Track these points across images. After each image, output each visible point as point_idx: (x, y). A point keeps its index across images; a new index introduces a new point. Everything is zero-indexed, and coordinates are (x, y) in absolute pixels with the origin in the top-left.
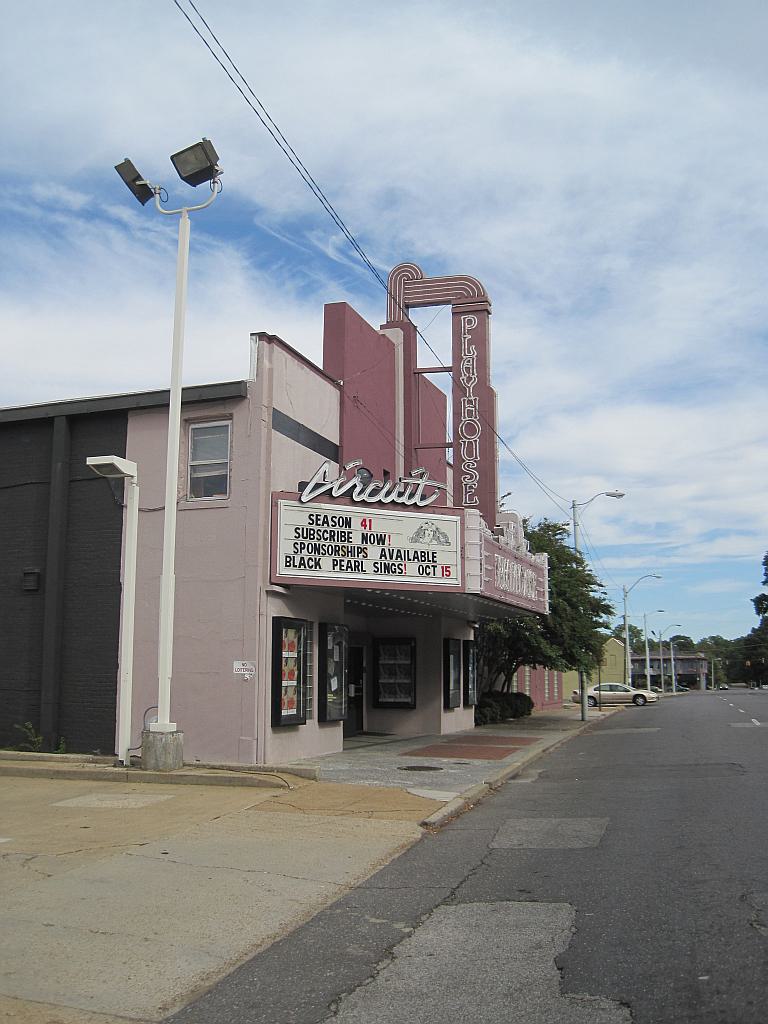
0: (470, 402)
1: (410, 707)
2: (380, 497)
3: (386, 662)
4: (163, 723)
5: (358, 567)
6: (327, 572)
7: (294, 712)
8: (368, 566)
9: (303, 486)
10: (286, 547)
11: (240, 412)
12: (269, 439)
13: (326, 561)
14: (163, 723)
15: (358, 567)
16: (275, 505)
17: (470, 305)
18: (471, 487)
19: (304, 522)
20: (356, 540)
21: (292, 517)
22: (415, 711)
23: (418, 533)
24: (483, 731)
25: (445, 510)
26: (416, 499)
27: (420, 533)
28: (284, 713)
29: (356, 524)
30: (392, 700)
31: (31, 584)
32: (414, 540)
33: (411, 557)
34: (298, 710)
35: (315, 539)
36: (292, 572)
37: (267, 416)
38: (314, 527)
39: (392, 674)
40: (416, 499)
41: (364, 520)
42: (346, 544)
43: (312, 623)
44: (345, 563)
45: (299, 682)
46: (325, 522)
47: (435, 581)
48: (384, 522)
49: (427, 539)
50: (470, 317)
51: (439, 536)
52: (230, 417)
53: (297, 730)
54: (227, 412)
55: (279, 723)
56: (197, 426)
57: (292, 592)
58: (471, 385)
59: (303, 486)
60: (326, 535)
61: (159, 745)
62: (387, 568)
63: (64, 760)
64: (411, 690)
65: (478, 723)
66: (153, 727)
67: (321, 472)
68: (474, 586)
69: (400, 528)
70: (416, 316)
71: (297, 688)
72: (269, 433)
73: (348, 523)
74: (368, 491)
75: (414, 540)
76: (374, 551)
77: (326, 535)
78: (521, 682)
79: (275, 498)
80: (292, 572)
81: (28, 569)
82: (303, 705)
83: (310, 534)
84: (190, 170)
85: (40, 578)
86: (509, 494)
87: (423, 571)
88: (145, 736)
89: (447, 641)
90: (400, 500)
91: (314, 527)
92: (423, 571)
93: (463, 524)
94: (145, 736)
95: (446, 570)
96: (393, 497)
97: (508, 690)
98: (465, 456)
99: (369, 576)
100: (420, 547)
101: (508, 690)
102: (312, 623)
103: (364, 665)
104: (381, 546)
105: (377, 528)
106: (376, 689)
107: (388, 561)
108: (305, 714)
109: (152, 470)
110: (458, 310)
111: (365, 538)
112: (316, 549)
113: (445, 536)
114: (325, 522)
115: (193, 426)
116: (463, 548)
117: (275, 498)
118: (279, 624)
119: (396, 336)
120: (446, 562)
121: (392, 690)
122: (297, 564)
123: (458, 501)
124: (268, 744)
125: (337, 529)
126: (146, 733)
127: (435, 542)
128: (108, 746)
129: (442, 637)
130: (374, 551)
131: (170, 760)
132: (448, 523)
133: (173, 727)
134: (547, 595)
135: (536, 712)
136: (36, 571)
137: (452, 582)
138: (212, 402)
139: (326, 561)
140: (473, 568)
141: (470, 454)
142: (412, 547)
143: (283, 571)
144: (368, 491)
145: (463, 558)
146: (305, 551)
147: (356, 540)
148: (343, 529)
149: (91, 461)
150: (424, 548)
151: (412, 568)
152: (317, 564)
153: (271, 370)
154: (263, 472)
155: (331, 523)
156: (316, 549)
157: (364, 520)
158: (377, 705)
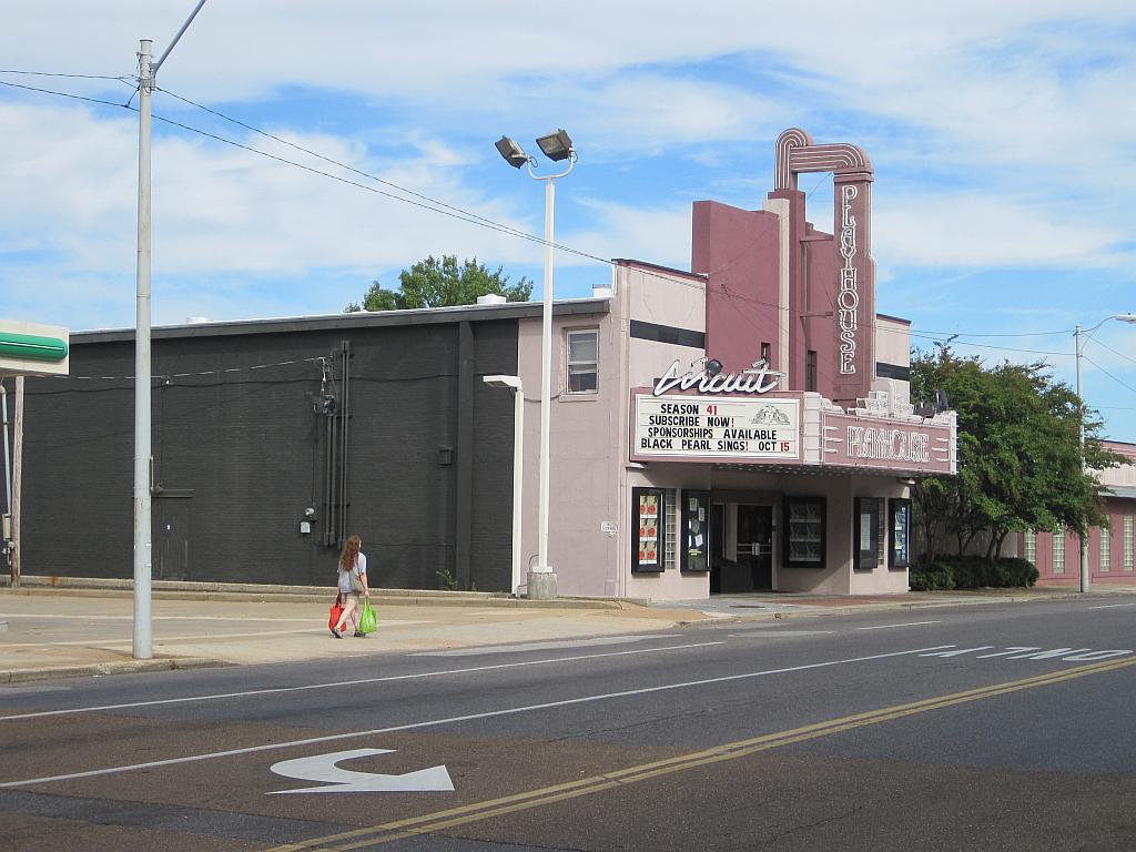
0: (849, 273)
1: (821, 565)
2: (724, 387)
3: (797, 521)
4: (543, 566)
5: (705, 446)
6: (678, 451)
7: (655, 562)
8: (713, 444)
9: (657, 381)
10: (642, 432)
11: (603, 323)
12: (628, 345)
13: (677, 442)
14: (543, 566)
15: (705, 446)
16: (633, 399)
17: (852, 174)
18: (848, 357)
19: (658, 411)
20: (703, 424)
21: (648, 408)
22: (825, 570)
23: (759, 416)
24: (914, 594)
25: (783, 395)
26: (757, 387)
27: (761, 415)
28: (641, 562)
29: (702, 411)
30: (802, 559)
31: (446, 459)
32: (756, 421)
33: (753, 436)
34: (658, 560)
35: (662, 426)
36: (647, 451)
37: (626, 327)
38: (666, 414)
39: (804, 534)
40: (757, 387)
41: (710, 407)
42: (694, 427)
43: (674, 490)
44: (692, 443)
45: (658, 538)
46: (676, 410)
47: (775, 455)
48: (726, 407)
49: (767, 420)
50: (848, 187)
51: (777, 415)
52: (598, 327)
53: (658, 576)
54: (595, 323)
55: (638, 570)
56: (573, 333)
57: (649, 467)
58: (851, 256)
59: (657, 381)
60: (676, 421)
61: (539, 581)
62: (730, 446)
63: (473, 596)
64: (821, 550)
65: (915, 586)
66: (535, 569)
67: (672, 369)
68: (812, 459)
69: (743, 412)
70: (805, 182)
71: (658, 543)
72: (628, 339)
73: (696, 410)
74: (713, 383)
75: (756, 421)
76: (718, 432)
77: (676, 421)
78: (1022, 545)
79: (633, 392)
80: (647, 451)
81: (444, 447)
82: (661, 556)
83: (661, 421)
84: (550, 149)
85: (454, 455)
86: (956, 336)
87: (763, 447)
88: (530, 578)
89: (857, 501)
90: (742, 389)
91: (666, 414)
92: (763, 447)
93: (802, 405)
94: (530, 578)
95: (785, 446)
96: (736, 386)
97: (998, 550)
98: (843, 326)
99: (714, 453)
100: (760, 427)
101: (998, 550)
102: (674, 490)
103: (773, 523)
104: (725, 428)
105: (721, 414)
106: (786, 549)
107: (732, 440)
108: (664, 563)
109: (543, 357)
110: (840, 180)
111: (710, 421)
112: (668, 433)
113: (785, 416)
114: (676, 410)
115: (570, 333)
116: (801, 427)
117: (633, 392)
118: (638, 493)
119: (782, 208)
120: (784, 439)
121: (802, 549)
122: (652, 445)
123: (792, 386)
124: (628, 586)
125: (686, 415)
126: (530, 574)
127: (775, 422)
128: (506, 586)
129: (853, 495)
130: (718, 432)
131: (547, 592)
132: (789, 406)
133: (550, 569)
134: (954, 456)
135: (1038, 583)
136: (450, 448)
137: (791, 456)
138: (581, 317)
139: (677, 442)
140: (812, 444)
141: (848, 323)
142: (753, 428)
143: (640, 451)
144: (713, 383)
145: (801, 434)
146: (658, 435)
147: (703, 424)
148: (691, 415)
149: (486, 379)
150: (765, 428)
151: (753, 444)
152: (669, 444)
153: (629, 288)
154: (623, 373)
155: (680, 411)
156: (668, 433)
157: (710, 407)
158: (787, 563)
